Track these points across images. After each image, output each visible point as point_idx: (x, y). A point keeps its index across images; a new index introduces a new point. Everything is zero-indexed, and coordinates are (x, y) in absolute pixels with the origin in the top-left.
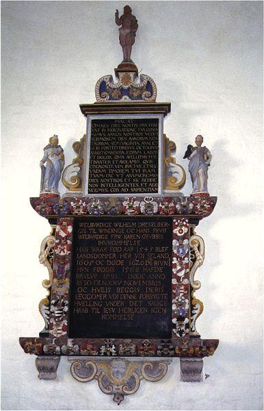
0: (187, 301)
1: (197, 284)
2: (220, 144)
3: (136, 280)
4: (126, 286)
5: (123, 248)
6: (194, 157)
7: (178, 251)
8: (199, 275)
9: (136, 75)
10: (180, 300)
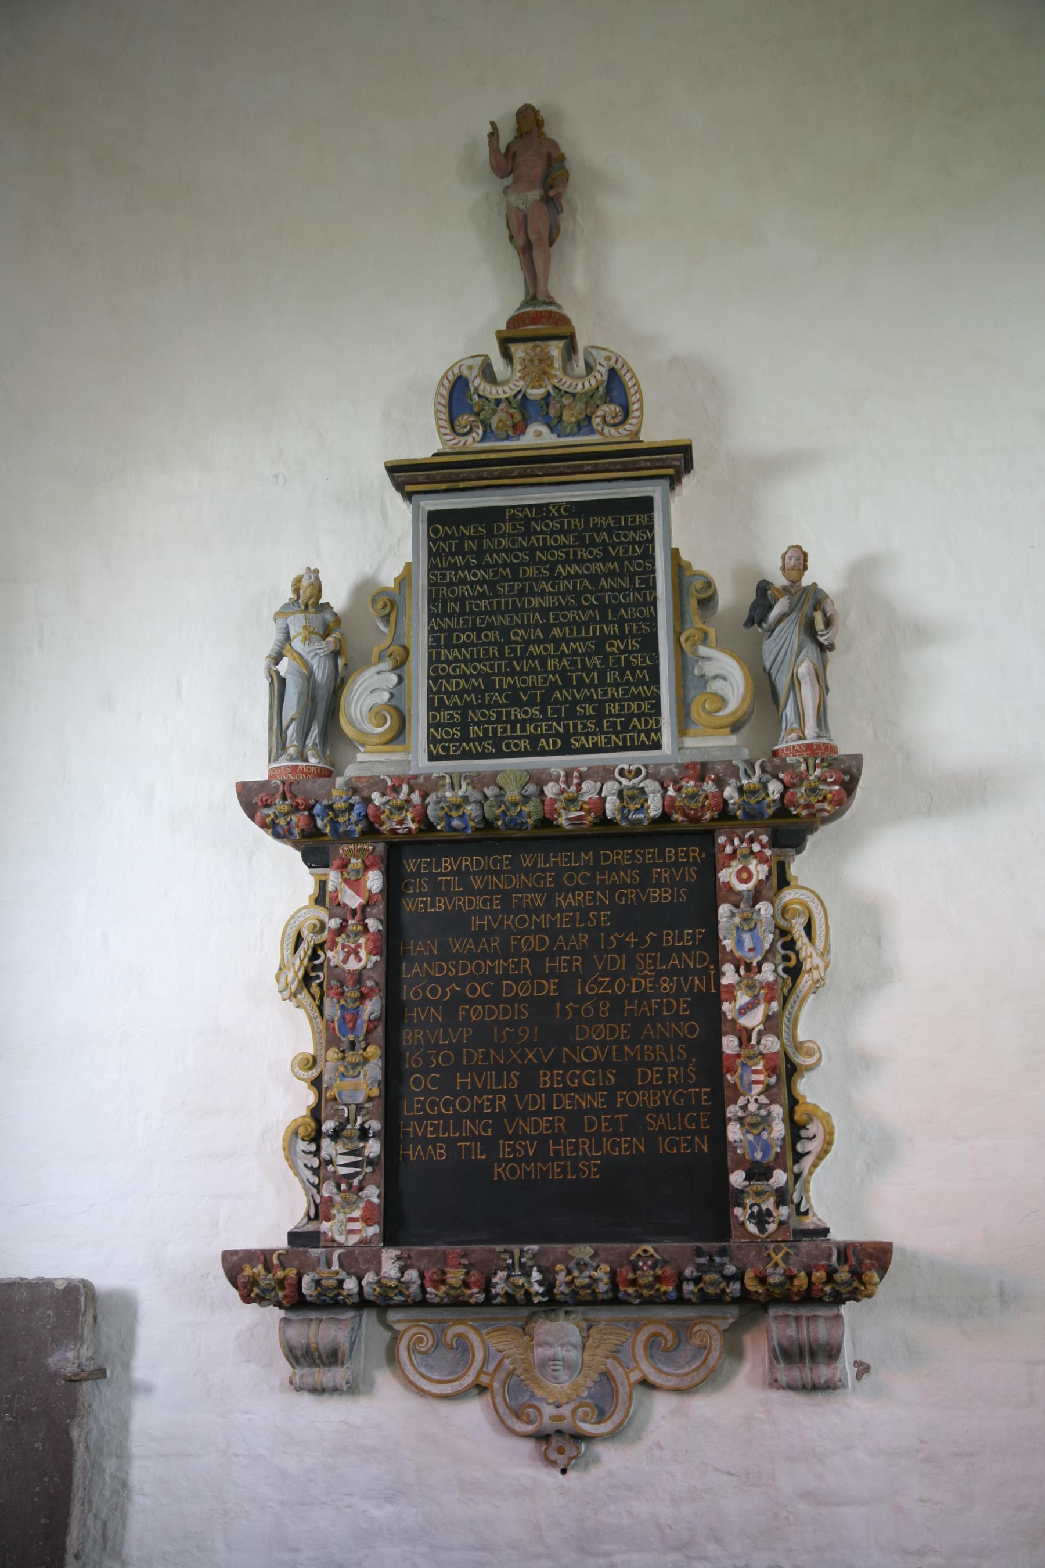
0: (777, 1110)
1: (809, 1053)
2: (865, 570)
3: (603, 1044)
4: (571, 1064)
5: (554, 939)
6: (779, 620)
7: (739, 943)
8: (810, 1024)
9: (571, 349)
10: (752, 1107)
